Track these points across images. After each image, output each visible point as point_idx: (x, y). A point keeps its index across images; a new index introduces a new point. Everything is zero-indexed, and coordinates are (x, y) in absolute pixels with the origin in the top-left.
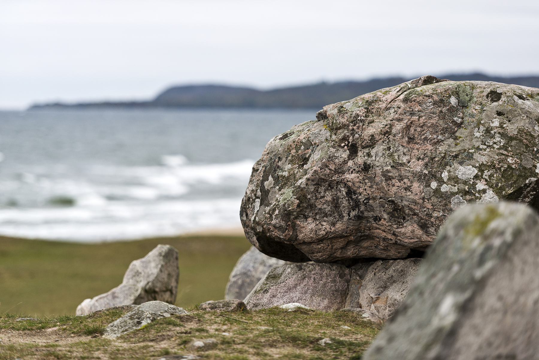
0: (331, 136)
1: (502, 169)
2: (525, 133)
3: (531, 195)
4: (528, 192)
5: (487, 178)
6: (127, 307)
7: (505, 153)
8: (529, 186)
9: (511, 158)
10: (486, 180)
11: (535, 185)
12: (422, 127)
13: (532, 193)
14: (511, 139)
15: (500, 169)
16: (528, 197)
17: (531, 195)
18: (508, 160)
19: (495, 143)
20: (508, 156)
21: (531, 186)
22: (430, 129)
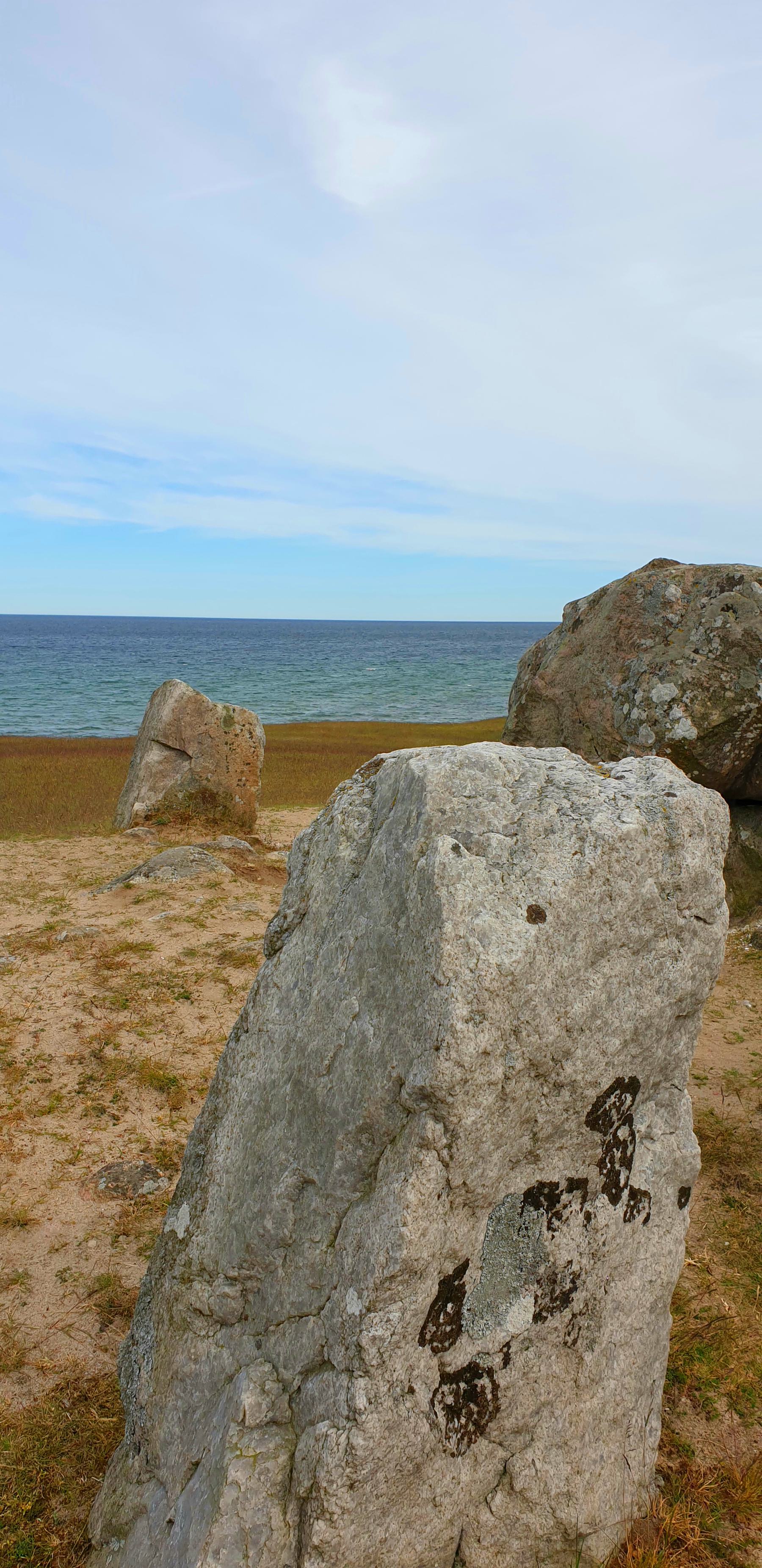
0: (312, 784)
1: (711, 690)
2: (752, 637)
3: (756, 729)
4: (749, 725)
5: (688, 701)
6: (94, 1495)
7: (720, 665)
8: (747, 717)
9: (726, 673)
10: (686, 706)
11: (757, 713)
12: (629, 628)
13: (755, 725)
14: (733, 644)
15: (708, 689)
16: (751, 731)
17: (756, 729)
18: (722, 676)
19: (710, 651)
20: (722, 670)
21: (751, 716)
22: (639, 631)
